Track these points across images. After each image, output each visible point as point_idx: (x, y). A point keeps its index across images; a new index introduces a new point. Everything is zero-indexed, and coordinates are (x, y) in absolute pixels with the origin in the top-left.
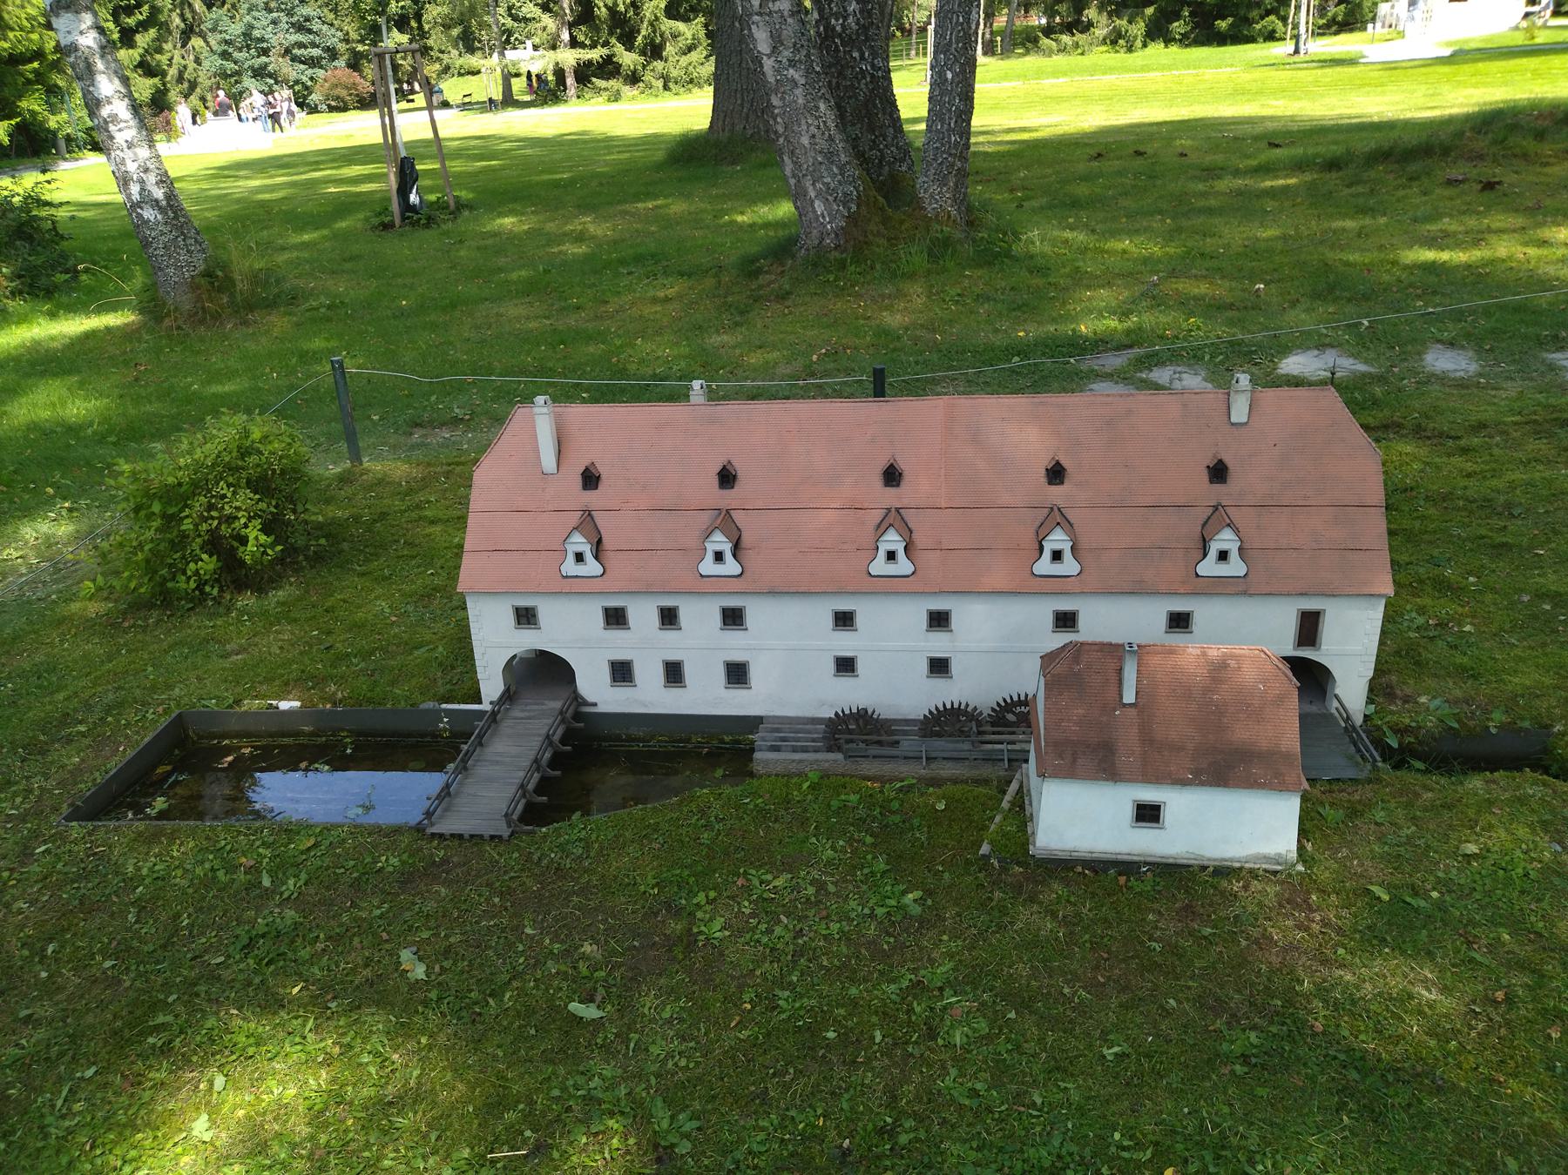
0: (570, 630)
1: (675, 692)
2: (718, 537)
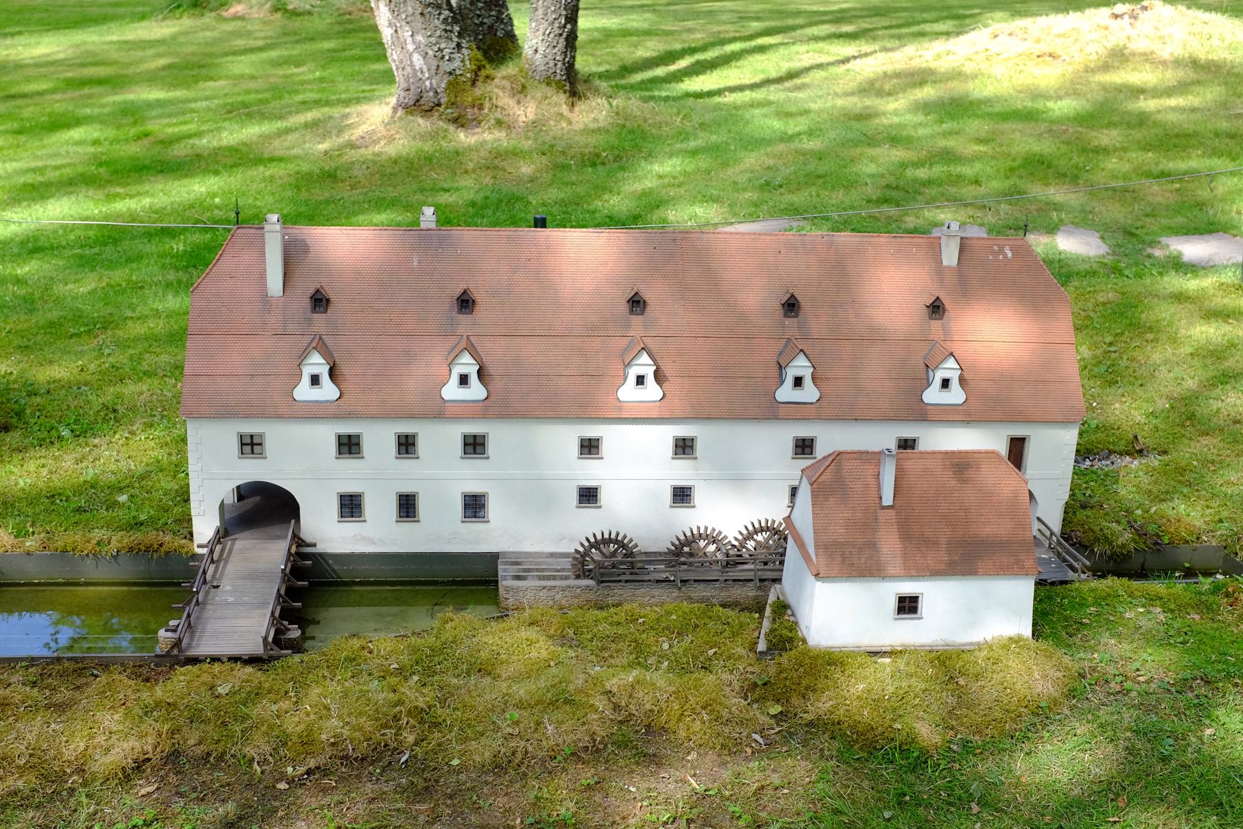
0: (300, 461)
1: (407, 527)
2: (466, 358)
